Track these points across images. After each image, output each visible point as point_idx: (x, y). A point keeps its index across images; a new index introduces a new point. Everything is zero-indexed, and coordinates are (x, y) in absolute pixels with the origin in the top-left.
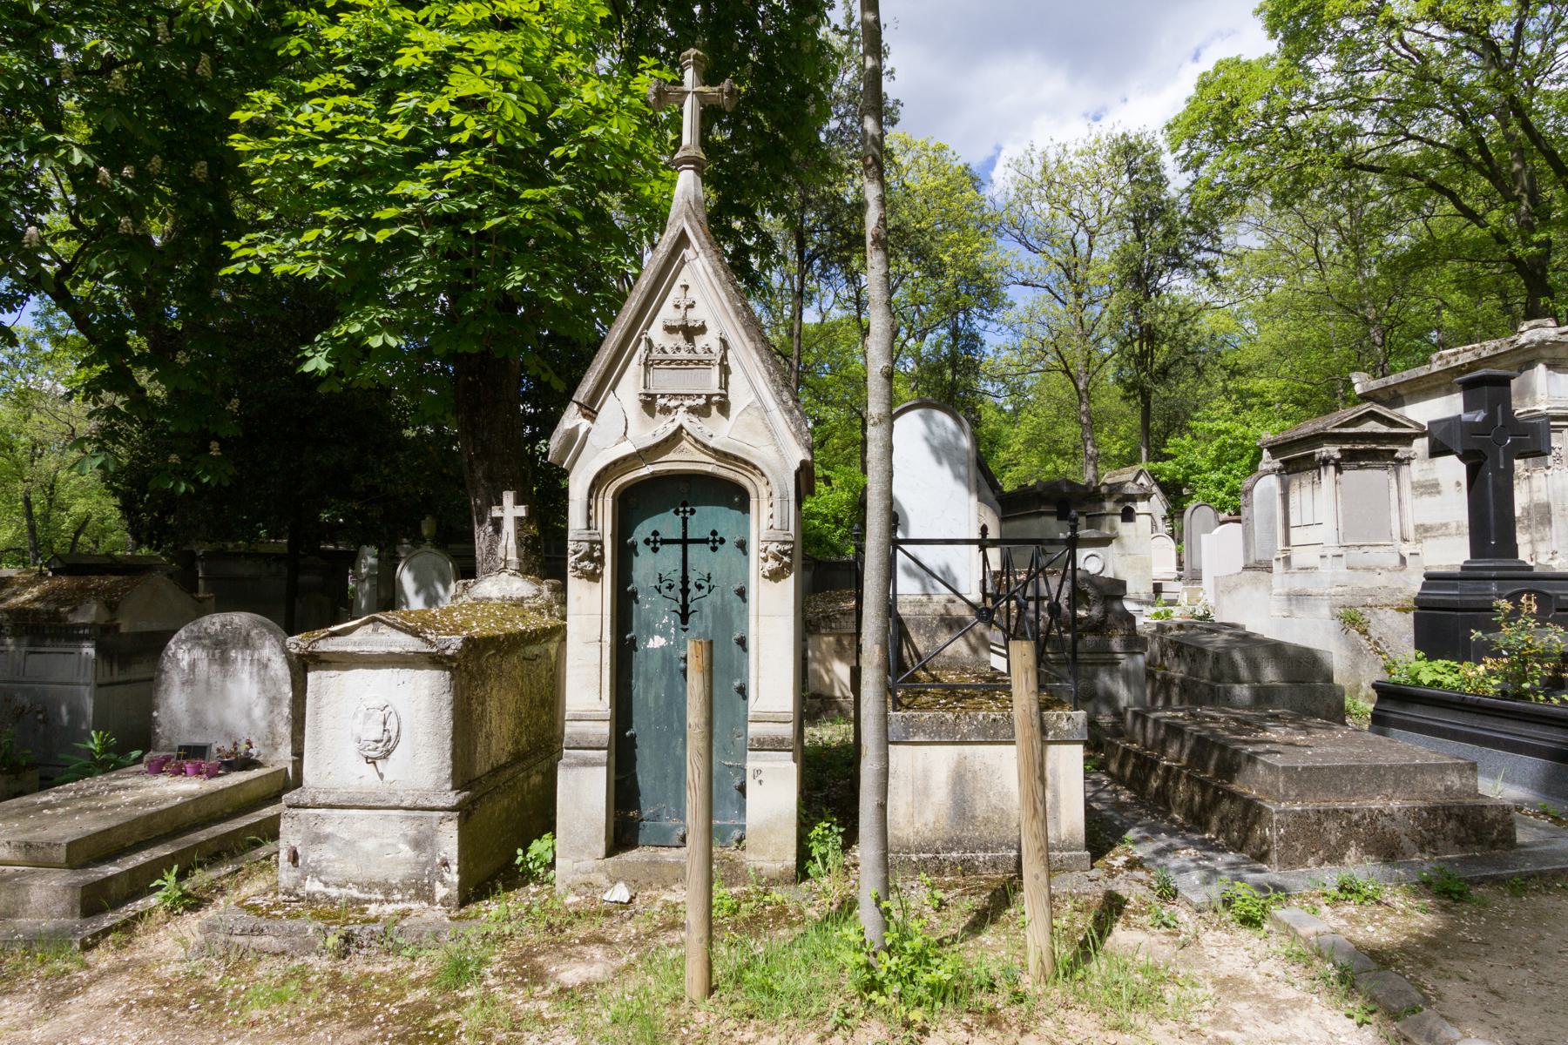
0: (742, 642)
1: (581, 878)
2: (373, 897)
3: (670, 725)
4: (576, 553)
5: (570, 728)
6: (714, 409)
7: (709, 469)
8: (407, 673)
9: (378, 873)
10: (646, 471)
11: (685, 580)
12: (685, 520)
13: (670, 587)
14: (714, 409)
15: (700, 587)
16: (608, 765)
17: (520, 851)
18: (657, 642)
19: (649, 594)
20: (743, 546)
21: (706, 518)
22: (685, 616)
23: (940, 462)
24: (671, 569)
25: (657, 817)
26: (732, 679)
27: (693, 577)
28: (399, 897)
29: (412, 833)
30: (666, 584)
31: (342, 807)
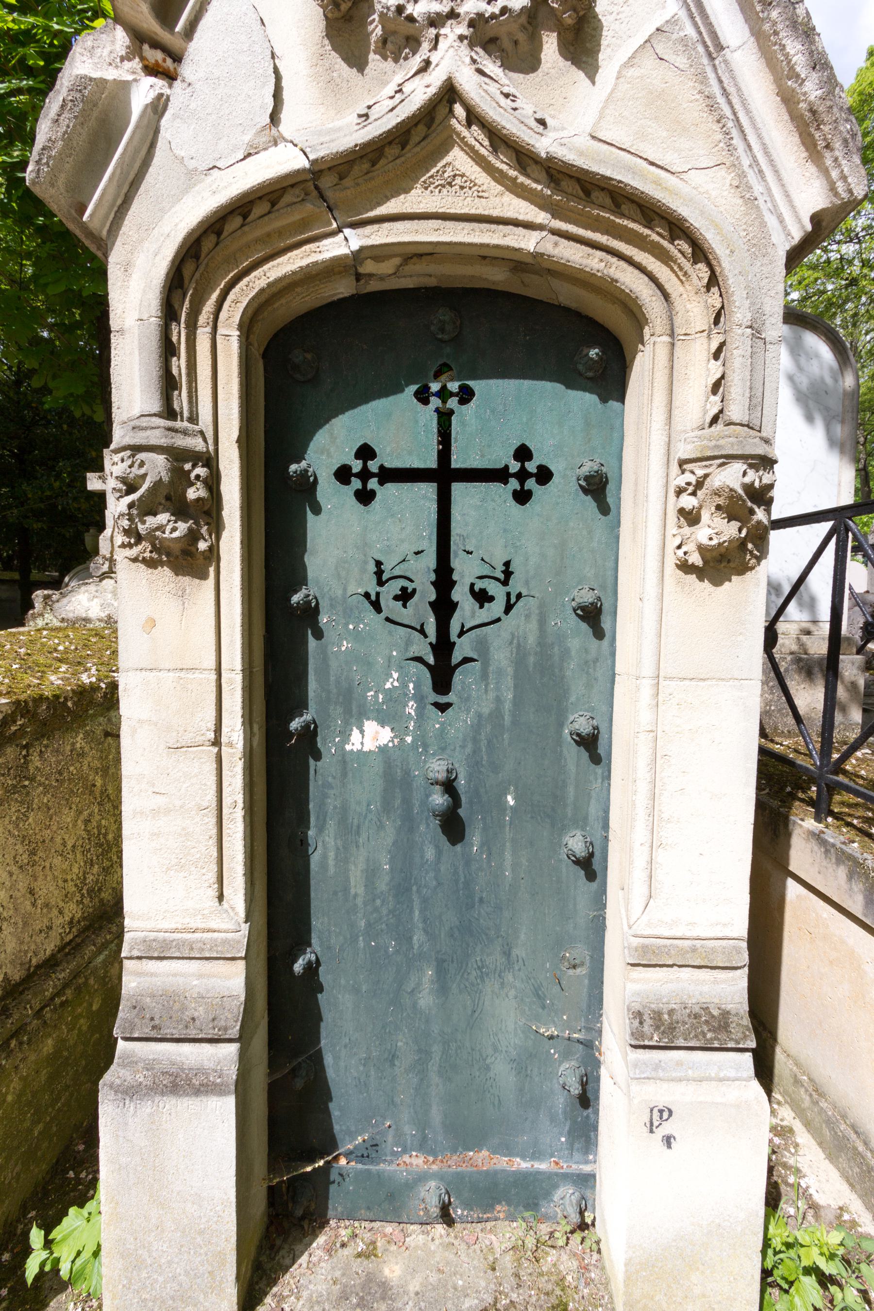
0: (592, 744)
3: (405, 938)
5: (136, 979)
6: (550, 44)
7: (528, 242)
11: (444, 578)
12: (445, 418)
13: (405, 596)
14: (550, 44)
15: (482, 597)
16: (243, 1039)
17: (36, 1236)
18: (371, 737)
19: (349, 614)
20: (598, 488)
21: (505, 413)
22: (442, 675)
23: (809, 419)
24: (408, 548)
25: (369, 1152)
26: (559, 827)
27: (466, 571)
30: (394, 588)
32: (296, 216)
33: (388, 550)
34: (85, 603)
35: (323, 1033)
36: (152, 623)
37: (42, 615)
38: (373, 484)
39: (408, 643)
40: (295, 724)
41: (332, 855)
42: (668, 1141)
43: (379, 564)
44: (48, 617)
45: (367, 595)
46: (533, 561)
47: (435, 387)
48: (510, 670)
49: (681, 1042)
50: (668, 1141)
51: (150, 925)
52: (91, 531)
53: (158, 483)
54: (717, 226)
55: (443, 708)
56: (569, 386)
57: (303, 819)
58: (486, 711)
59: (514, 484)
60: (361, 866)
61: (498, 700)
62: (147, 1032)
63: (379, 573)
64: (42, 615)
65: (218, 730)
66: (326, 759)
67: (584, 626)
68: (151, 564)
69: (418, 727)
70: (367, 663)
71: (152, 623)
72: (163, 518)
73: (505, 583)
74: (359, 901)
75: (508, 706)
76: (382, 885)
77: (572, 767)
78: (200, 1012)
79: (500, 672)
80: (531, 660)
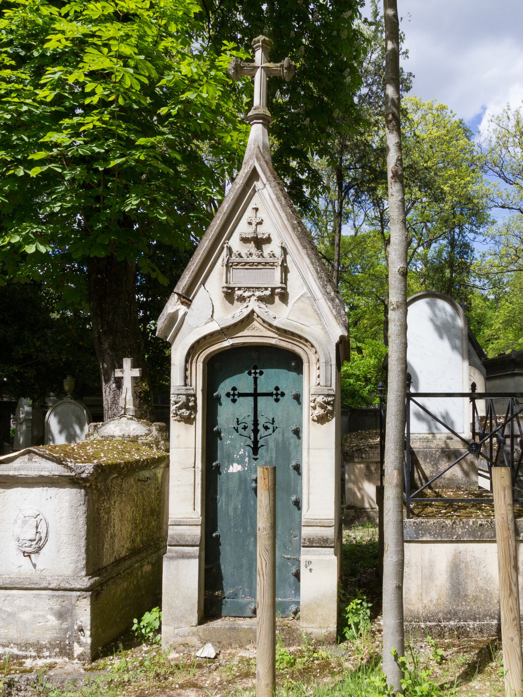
0: (297, 468)
1: (180, 640)
2: (28, 654)
3: (245, 529)
4: (176, 403)
5: (172, 531)
6: (277, 298)
7: (273, 342)
8: (53, 491)
9: (31, 637)
10: (227, 343)
11: (256, 423)
12: (256, 379)
13: (245, 428)
14: (277, 298)
15: (266, 428)
17: (135, 621)
18: (235, 468)
19: (229, 433)
20: (298, 398)
21: (272, 378)
22: (255, 449)
24: (245, 415)
26: (290, 495)
27: (262, 421)
28: (47, 654)
29: (57, 607)
30: (242, 426)
31: (6, 589)
32: (217, 338)
33: (240, 415)
34: (113, 429)
35: (221, 558)
36: (179, 436)
37: (93, 434)
38: (275, 392)
39: (246, 441)
40: (214, 464)
41: (224, 503)
42: (311, 570)
43: (238, 419)
44: (96, 435)
45: (234, 428)
46: (280, 418)
47: (253, 371)
48: (274, 449)
49: (315, 545)
50: (311, 570)
51: (176, 517)
52: (68, 378)
53: (184, 403)
54: (316, 340)
55: (256, 459)
56: (289, 371)
57: (216, 493)
58: (268, 460)
59: (275, 397)
60: (233, 506)
61: (271, 457)
62: (175, 543)
63: (238, 422)
64: (93, 434)
65: (195, 464)
66: (222, 475)
67: (295, 436)
68: (179, 421)
69: (249, 465)
70: (234, 447)
71: (179, 436)
72: (184, 410)
73: (273, 424)
74: (232, 517)
75: (274, 459)
76: (239, 512)
77: (292, 476)
78: (189, 539)
79: (272, 449)
80: (280, 445)
